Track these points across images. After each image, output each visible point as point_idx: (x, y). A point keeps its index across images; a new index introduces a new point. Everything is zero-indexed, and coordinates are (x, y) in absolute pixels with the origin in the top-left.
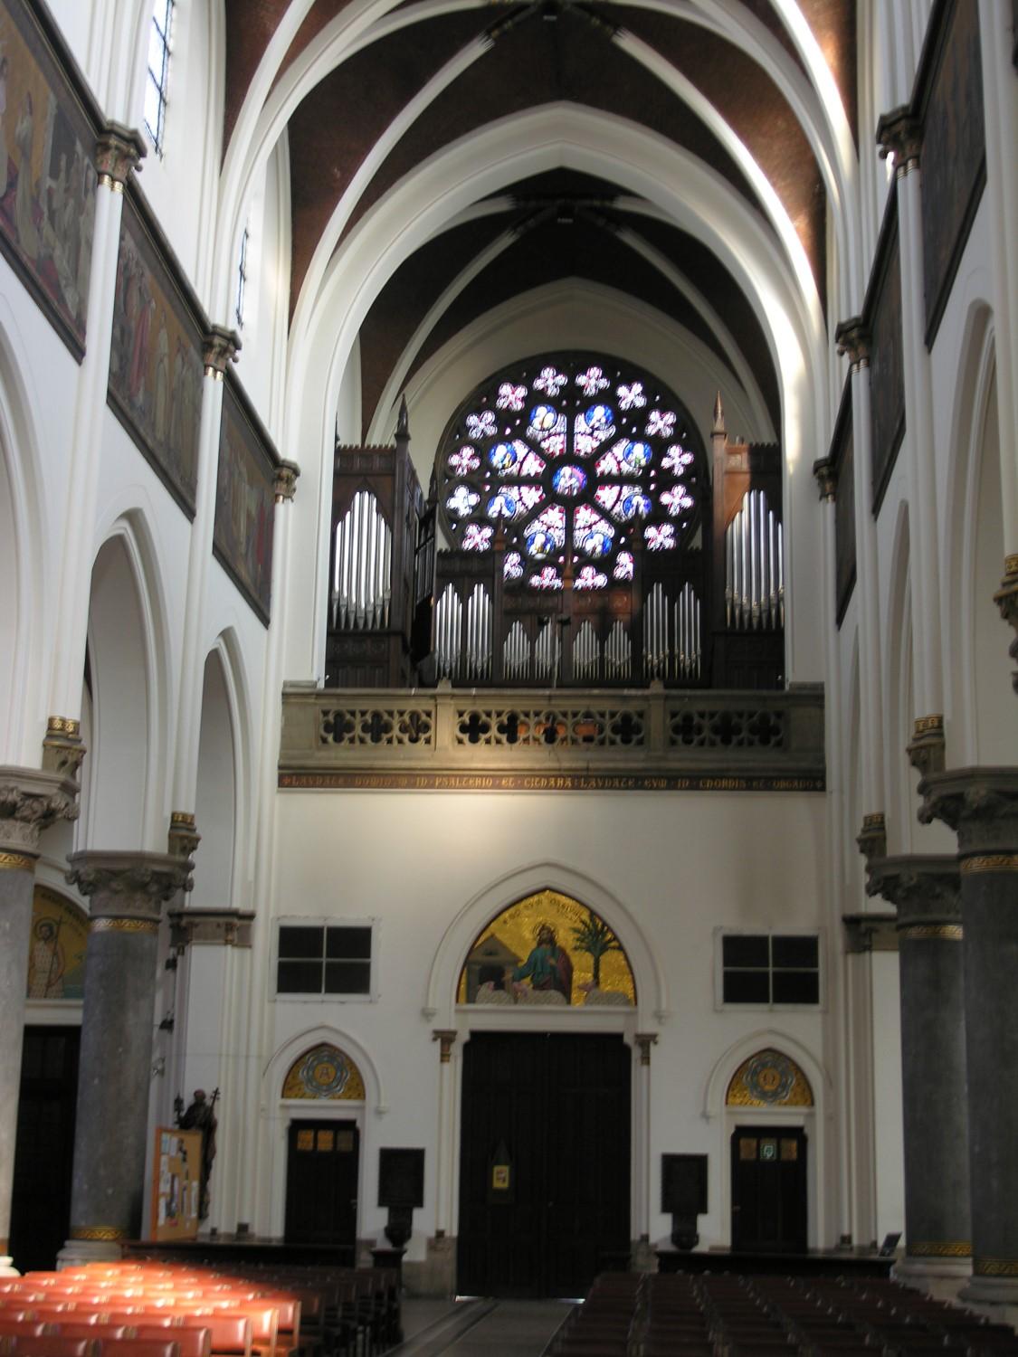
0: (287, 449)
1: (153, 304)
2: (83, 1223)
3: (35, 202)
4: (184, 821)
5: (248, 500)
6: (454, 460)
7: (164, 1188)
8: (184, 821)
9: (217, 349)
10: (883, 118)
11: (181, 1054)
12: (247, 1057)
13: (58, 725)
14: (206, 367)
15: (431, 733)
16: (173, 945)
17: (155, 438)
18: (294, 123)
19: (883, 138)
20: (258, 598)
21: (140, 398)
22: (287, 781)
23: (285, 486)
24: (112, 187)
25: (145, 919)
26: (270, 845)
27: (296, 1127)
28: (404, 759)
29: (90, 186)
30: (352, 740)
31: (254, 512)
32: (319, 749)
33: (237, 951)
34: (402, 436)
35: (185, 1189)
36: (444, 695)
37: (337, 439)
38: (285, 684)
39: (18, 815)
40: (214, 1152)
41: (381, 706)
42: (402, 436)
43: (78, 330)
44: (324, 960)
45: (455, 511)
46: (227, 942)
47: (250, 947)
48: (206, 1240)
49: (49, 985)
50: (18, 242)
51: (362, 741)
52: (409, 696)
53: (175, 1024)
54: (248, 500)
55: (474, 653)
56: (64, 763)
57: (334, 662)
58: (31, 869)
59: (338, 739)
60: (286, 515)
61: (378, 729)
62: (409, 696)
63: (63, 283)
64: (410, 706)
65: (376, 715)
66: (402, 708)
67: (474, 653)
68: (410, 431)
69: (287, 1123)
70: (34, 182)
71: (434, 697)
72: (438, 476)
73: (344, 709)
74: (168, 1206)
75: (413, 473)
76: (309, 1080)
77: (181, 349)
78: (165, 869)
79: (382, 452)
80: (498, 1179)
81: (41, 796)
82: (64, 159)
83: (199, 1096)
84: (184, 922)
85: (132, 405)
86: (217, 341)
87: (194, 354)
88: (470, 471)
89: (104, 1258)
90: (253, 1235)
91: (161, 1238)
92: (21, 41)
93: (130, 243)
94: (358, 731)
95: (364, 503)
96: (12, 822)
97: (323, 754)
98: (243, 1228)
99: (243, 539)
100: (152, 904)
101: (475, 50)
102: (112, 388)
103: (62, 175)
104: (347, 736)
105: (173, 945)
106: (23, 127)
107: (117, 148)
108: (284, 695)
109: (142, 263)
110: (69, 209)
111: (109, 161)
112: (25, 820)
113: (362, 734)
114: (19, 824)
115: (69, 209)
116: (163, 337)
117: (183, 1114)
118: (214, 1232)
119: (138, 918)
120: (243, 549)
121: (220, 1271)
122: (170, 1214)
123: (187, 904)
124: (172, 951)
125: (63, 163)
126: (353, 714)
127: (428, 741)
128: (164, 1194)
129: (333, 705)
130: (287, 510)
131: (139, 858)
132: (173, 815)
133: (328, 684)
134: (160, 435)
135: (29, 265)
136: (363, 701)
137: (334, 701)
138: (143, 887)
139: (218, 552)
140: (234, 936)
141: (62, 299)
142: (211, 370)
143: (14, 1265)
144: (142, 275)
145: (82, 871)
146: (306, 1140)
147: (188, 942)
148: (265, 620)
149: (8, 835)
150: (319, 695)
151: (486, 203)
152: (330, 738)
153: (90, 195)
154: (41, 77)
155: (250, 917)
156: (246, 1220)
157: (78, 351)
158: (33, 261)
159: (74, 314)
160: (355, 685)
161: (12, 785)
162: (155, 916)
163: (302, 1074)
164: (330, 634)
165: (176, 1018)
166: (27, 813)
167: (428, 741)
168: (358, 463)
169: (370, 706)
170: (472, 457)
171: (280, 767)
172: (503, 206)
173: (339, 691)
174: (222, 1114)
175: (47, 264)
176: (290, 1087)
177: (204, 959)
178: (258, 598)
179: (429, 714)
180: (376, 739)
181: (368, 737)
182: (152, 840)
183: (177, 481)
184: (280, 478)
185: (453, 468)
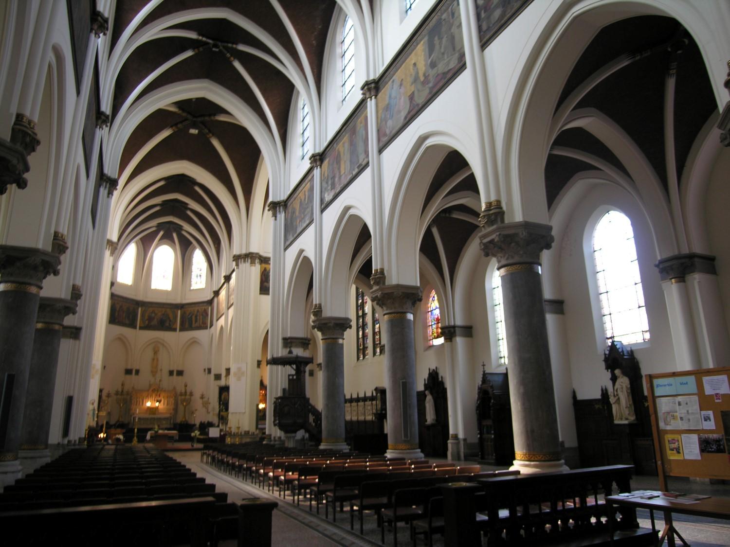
10: (313, 154)
19: (312, 159)
80: (672, 450)
86: (103, 117)
101: (189, 54)
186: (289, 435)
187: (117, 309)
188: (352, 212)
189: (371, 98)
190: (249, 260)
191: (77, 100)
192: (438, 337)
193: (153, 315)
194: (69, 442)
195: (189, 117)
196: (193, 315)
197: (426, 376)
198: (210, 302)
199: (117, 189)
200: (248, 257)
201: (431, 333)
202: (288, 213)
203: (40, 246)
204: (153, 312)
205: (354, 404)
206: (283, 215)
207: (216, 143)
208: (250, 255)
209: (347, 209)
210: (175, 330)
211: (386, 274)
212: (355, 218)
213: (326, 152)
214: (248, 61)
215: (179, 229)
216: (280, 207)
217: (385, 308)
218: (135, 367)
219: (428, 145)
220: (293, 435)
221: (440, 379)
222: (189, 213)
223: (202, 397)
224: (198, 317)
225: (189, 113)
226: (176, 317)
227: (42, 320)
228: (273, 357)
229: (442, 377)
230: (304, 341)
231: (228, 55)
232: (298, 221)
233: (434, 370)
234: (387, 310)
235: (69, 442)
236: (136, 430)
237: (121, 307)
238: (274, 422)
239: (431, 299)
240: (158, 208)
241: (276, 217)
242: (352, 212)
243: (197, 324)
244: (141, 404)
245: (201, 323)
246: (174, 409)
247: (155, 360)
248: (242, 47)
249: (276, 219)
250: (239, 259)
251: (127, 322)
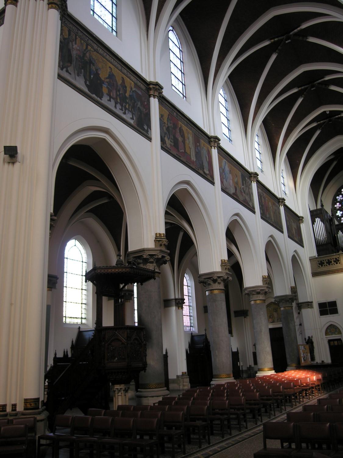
0: (300, 214)
1: (267, 199)
2: (289, 363)
3: (241, 191)
4: (293, 288)
5: (294, 226)
6: (336, 206)
7: (302, 355)
8: (293, 288)
9: (281, 202)
11: (304, 330)
12: (317, 329)
13: (264, 277)
14: (280, 205)
15: (340, 261)
16: (298, 310)
17: (272, 221)
18: (287, 154)
20: (300, 242)
21: (268, 216)
22: (314, 275)
23: (301, 221)
24: (254, 183)
25: (290, 307)
26: (313, 288)
27: (330, 341)
28: (335, 267)
29: (250, 184)
30: (324, 266)
31: (296, 227)
32: (318, 268)
33: (311, 309)
34: (322, 206)
35: (307, 355)
36: (340, 254)
37: (310, 209)
38: (310, 257)
39: (260, 293)
40: (314, 347)
41: (329, 258)
42: (322, 206)
43: (253, 209)
44: (328, 308)
45: (338, 216)
46: (308, 308)
47: (313, 308)
48: (316, 364)
49: (278, 320)
50: (239, 199)
51: (327, 265)
52: (334, 255)
53: (302, 324)
54: (294, 226)
55: (25, 416)
56: (266, 283)
57: (319, 251)
58: (265, 302)
59: (322, 266)
60: (303, 226)
61: (329, 263)
62: (334, 255)
63: (249, 202)
64: (335, 257)
65: (328, 260)
66: (333, 258)
67: (25, 416)
68: (324, 205)
69: (327, 340)
70: (240, 188)
71: (339, 254)
72: (333, 210)
73: (322, 260)
74: (304, 359)
75: (326, 212)
76: (330, 332)
77: (274, 204)
78: (291, 297)
79: (320, 210)
81: (264, 290)
82: (244, 181)
83: (309, 337)
84: (300, 305)
85: (266, 217)
86: (281, 200)
87: (277, 204)
88: (339, 207)
89: (293, 370)
90: (325, 363)
91: (303, 365)
92: (232, 166)
93: (260, 190)
94: (325, 264)
95: (318, 220)
96: (259, 295)
97: (319, 269)
98: (323, 361)
99: (295, 233)
100: (291, 304)
102: (261, 216)
103: (245, 185)
104: (323, 265)
105: (298, 310)
106: (236, 180)
107: (253, 176)
108: (310, 259)
109: (263, 192)
110: (247, 189)
111: (252, 178)
112: (262, 294)
113: (326, 264)
114: (261, 295)
115: (247, 189)
116: (270, 203)
117: (307, 341)
118: (317, 363)
119: (288, 307)
120: (295, 235)
121: (312, 370)
122: (304, 360)
123: (299, 302)
124: (299, 311)
125: (244, 183)
126: (324, 260)
127: (340, 263)
128: (302, 357)
129: (319, 260)
130: (303, 225)
131: (286, 296)
132: (291, 287)
133: (318, 256)
134: (273, 221)
135: (242, 202)
136: (325, 258)
137: (319, 259)
138: (288, 301)
139: (289, 237)
140: (310, 306)
141: (249, 205)
142: (281, 206)
143: (275, 372)
144: (263, 194)
145: (276, 300)
146: (332, 343)
147: (301, 309)
148: (303, 247)
149: (259, 297)
150: (316, 258)
151: (329, 157)
152: (320, 266)
153: (250, 185)
154: (237, 171)
155: (312, 302)
156: (323, 360)
157: (254, 212)
158: (242, 201)
159: (252, 206)
160: (323, 255)
161: (258, 289)
162: (292, 306)
163: (328, 331)
164: (316, 246)
165: (302, 323)
166: (262, 293)
167: (340, 263)
168: (315, 213)
169: (327, 258)
170: (339, 205)
171: (312, 273)
172: (332, 157)
173: (320, 257)
174: (314, 340)
175: (245, 201)
176: (327, 333)
177: (305, 312)
178: (300, 242)
179: (339, 258)
180: (329, 265)
181: (328, 265)
182: (288, 292)
183: (278, 227)
184: (300, 220)
185: (336, 207)
214: (316, 31)
231: (301, 38)
248: (327, 78)
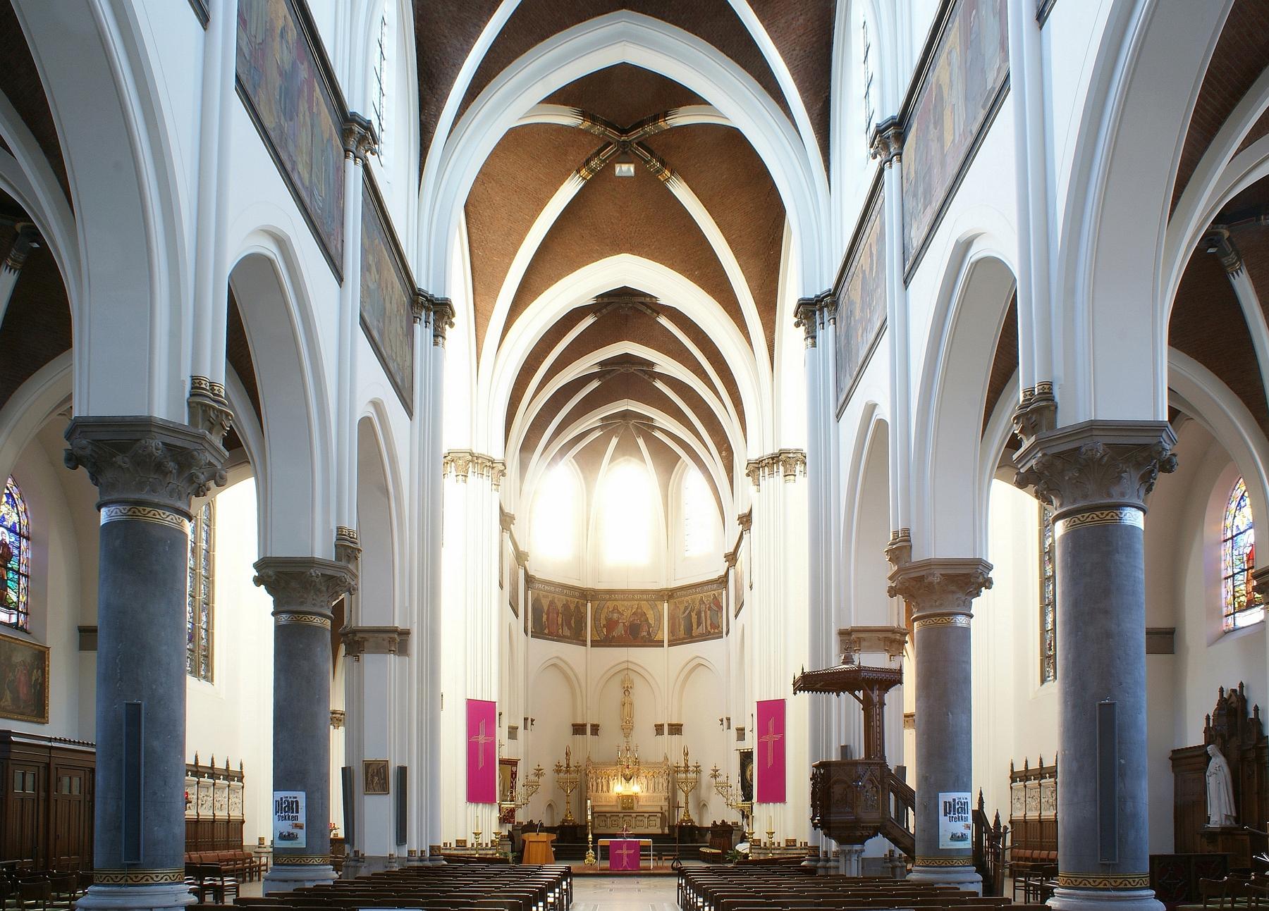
186: (847, 848)
187: (546, 608)
188: (975, 253)
189: (891, 161)
190: (781, 468)
191: (205, 37)
192: (1251, 604)
193: (615, 616)
194: (410, 852)
195: (612, 134)
196: (692, 610)
197: (1211, 706)
198: (723, 581)
199: (452, 325)
200: (778, 462)
201: (1230, 597)
202: (841, 318)
203: (161, 411)
204: (615, 609)
205: (1032, 783)
206: (831, 328)
207: (682, 192)
208: (783, 457)
209: (964, 246)
210: (660, 644)
211: (1057, 399)
212: (992, 265)
213: (910, 110)
215: (646, 427)
216: (821, 310)
217: (1056, 502)
218: (590, 720)
219: (972, 260)
220: (857, 847)
221: (1252, 715)
222: (659, 385)
223: (715, 776)
224: (703, 615)
225: (608, 124)
226: (659, 619)
227: (286, 608)
228: (803, 673)
229: (1256, 709)
230: (890, 635)
232: (860, 331)
233: (1234, 691)
234: (1061, 505)
235: (410, 852)
236: (590, 836)
237: (552, 603)
238: (813, 819)
239: (1234, 505)
240: (595, 384)
241: (814, 337)
242: (975, 253)
243: (702, 629)
244: (605, 789)
245: (709, 628)
246: (667, 799)
247: (627, 705)
249: (814, 345)
250: (759, 468)
251: (567, 633)
